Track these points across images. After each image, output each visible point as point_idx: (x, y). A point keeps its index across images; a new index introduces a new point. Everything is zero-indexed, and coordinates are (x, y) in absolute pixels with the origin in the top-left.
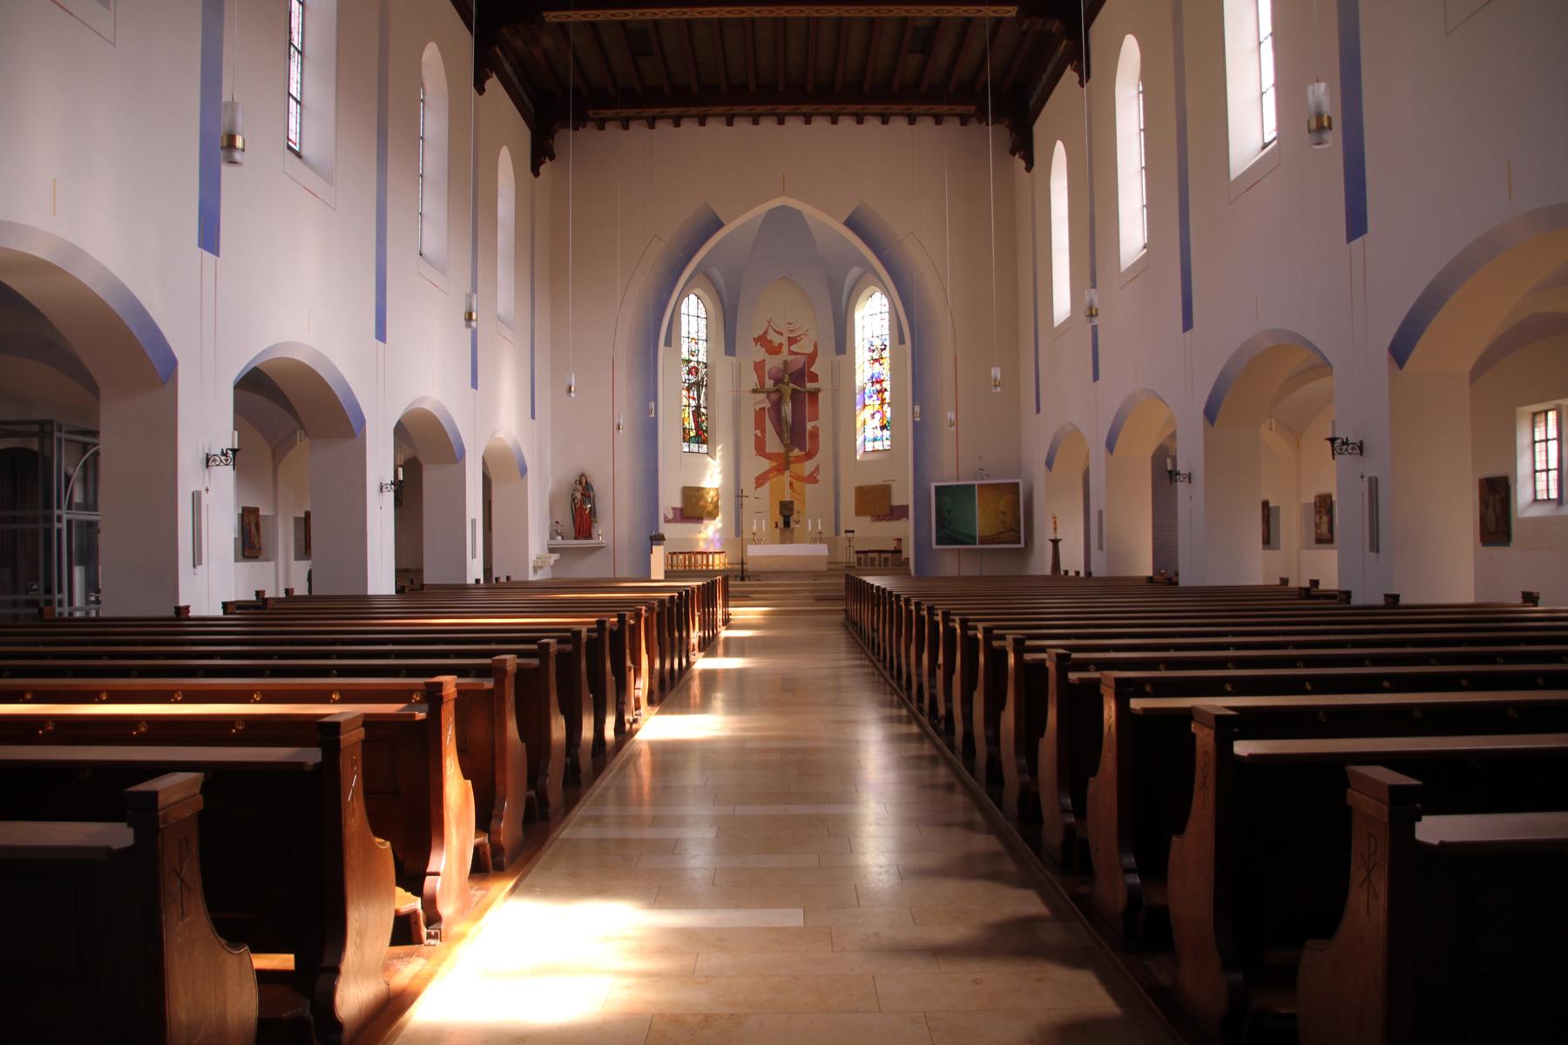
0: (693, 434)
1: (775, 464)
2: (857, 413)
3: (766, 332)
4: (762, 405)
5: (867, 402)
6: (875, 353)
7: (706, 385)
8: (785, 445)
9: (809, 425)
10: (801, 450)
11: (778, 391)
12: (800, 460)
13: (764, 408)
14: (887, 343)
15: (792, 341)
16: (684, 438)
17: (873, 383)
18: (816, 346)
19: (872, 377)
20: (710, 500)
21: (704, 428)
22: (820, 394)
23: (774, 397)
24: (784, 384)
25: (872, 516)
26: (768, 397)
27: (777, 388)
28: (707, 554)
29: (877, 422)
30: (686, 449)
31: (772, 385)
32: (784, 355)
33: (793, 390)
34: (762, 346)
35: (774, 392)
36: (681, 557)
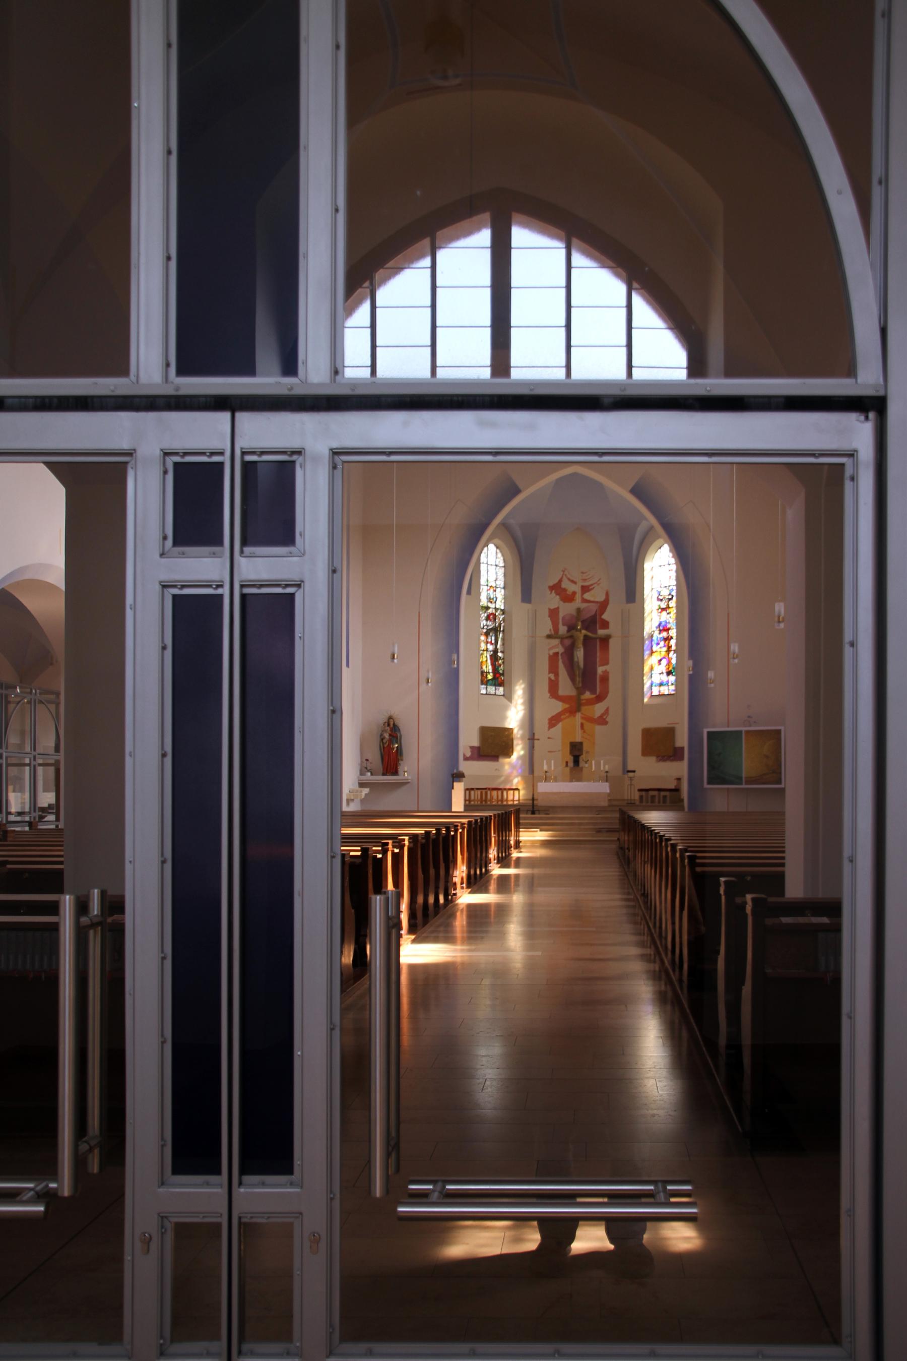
0: (490, 677)
1: (567, 706)
3: (560, 581)
5: (655, 648)
6: (664, 602)
7: (503, 631)
8: (577, 688)
9: (600, 670)
15: (585, 589)
18: (607, 594)
19: (660, 625)
21: (501, 672)
23: (568, 642)
26: (562, 643)
27: (569, 634)
28: (502, 790)
29: (663, 667)
30: (484, 692)
31: (565, 632)
32: (578, 603)
35: (567, 638)
36: (479, 792)
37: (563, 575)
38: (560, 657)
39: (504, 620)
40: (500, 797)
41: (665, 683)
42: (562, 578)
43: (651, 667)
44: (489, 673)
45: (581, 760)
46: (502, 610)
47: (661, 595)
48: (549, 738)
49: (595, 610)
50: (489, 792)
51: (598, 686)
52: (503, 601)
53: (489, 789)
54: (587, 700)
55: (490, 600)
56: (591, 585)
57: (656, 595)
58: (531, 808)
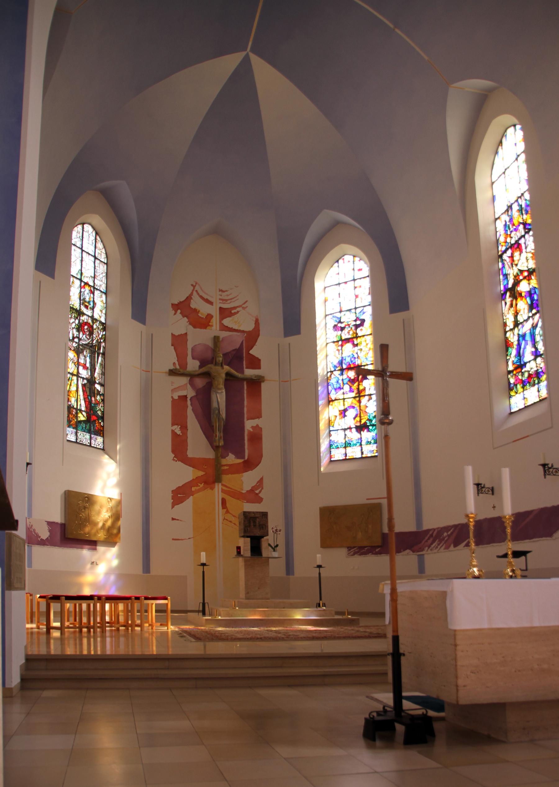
0: (82, 417)
1: (200, 473)
2: (320, 409)
3: (189, 298)
4: (183, 393)
5: (333, 396)
6: (346, 331)
7: (103, 354)
8: (216, 448)
9: (249, 425)
10: (238, 457)
11: (207, 374)
12: (235, 470)
13: (186, 397)
14: (368, 316)
15: (225, 313)
16: (69, 421)
17: (342, 370)
18: (257, 322)
19: (341, 363)
20: (100, 524)
21: (99, 413)
22: (263, 385)
23: (200, 383)
24: (216, 364)
25: (349, 548)
26: (191, 383)
27: (204, 369)
29: (350, 420)
30: (72, 438)
31: (197, 368)
32: (215, 330)
33: (228, 374)
34: (184, 316)
35: (199, 375)
37: (193, 290)
38: (189, 402)
39: (105, 338)
41: (355, 442)
42: (192, 294)
43: (327, 422)
44: (81, 411)
45: (264, 543)
46: (102, 324)
47: (343, 322)
48: (173, 519)
49: (240, 342)
51: (246, 447)
52: (104, 311)
53: (99, 598)
54: (230, 465)
55: (83, 301)
56: (235, 308)
57: (331, 322)
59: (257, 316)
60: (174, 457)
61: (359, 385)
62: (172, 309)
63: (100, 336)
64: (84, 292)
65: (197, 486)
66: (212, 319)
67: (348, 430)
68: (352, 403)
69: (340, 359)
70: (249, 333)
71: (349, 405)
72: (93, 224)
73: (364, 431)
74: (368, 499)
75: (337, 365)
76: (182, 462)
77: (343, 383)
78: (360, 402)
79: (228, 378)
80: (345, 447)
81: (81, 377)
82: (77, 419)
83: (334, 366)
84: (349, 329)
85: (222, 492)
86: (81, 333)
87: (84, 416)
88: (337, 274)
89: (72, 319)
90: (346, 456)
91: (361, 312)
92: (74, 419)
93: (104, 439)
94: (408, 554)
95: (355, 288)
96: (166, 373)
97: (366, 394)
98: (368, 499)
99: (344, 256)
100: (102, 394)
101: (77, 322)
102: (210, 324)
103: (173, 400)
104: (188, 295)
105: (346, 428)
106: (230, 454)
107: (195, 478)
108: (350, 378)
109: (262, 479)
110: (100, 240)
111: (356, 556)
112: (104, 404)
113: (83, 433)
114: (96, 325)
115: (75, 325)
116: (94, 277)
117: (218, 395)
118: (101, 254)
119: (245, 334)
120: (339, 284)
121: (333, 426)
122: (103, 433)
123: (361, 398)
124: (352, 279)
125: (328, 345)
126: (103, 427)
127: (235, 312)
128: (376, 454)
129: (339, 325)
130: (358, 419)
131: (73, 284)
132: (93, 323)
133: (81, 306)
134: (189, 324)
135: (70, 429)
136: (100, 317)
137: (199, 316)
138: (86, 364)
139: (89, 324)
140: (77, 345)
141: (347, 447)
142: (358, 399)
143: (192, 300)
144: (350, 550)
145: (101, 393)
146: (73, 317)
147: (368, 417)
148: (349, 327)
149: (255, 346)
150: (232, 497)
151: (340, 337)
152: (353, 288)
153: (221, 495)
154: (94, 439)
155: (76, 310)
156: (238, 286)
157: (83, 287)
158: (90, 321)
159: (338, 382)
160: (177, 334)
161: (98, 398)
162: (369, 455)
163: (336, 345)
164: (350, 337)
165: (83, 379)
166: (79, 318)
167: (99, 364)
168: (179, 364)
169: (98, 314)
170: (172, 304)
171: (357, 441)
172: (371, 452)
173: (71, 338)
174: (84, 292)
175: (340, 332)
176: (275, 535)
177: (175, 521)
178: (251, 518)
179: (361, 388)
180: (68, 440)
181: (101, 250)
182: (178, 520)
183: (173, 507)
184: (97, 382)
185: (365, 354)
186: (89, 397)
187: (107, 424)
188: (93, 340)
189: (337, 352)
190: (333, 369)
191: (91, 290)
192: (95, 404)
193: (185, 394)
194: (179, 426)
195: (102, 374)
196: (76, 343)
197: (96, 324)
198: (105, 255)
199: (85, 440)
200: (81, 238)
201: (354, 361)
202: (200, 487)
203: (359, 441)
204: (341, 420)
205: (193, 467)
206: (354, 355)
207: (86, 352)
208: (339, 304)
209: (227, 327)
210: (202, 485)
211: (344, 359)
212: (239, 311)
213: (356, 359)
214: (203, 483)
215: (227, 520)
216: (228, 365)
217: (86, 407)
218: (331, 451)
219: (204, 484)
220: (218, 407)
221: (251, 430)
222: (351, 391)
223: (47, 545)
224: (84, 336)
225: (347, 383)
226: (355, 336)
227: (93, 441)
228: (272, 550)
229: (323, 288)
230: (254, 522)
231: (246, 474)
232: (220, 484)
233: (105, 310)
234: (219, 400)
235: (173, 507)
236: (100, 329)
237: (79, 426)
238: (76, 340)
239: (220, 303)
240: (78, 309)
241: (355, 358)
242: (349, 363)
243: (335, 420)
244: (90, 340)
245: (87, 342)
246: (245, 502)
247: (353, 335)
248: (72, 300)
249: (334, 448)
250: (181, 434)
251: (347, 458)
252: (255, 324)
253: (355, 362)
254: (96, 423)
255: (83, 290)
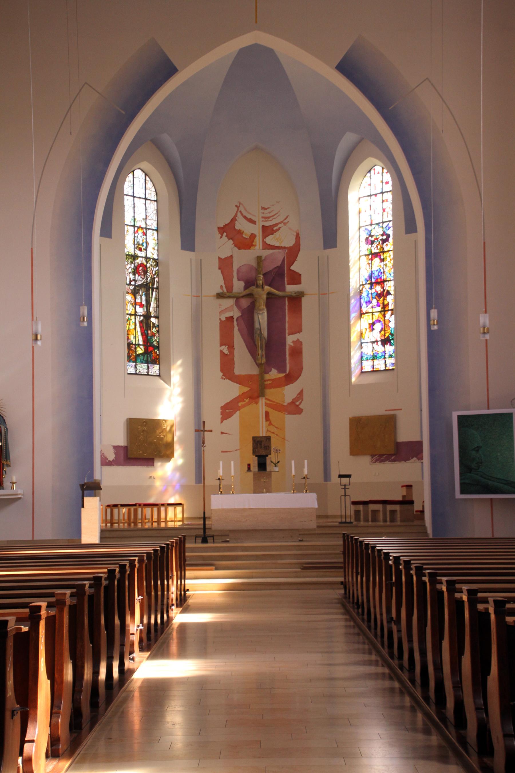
0: (140, 351)
1: (246, 389)
3: (234, 220)
5: (364, 309)
6: (375, 245)
7: (157, 288)
8: (259, 365)
9: (290, 340)
11: (250, 295)
12: (278, 384)
13: (232, 317)
15: (267, 231)
16: (129, 356)
17: (371, 284)
18: (298, 237)
19: (370, 277)
21: (155, 344)
22: (304, 300)
23: (245, 303)
24: (257, 286)
25: (372, 456)
26: (237, 304)
27: (248, 291)
29: (376, 335)
30: (133, 371)
32: (258, 250)
33: (269, 294)
36: (124, 510)
37: (238, 211)
38: (235, 323)
40: (109, 518)
41: (380, 355)
42: (236, 215)
43: (359, 334)
44: (139, 345)
47: (373, 236)
48: (222, 433)
50: (140, 510)
51: (288, 361)
52: (156, 248)
56: (276, 225)
57: (364, 235)
58: (201, 532)
59: (298, 230)
60: (223, 375)
61: (384, 300)
62: (218, 233)
63: (154, 273)
64: (137, 236)
65: (244, 401)
66: (255, 239)
67: (376, 343)
68: (379, 317)
69: (370, 272)
70: (290, 249)
71: (376, 319)
72: (142, 168)
73: (387, 345)
74: (386, 410)
75: (368, 279)
76: (230, 379)
77: (372, 297)
78: (384, 316)
79: (270, 296)
80: (373, 360)
81: (138, 315)
82: (136, 353)
83: (365, 279)
84: (378, 243)
85: (265, 405)
86: (137, 275)
87: (142, 350)
88: (369, 185)
89: (128, 265)
90: (373, 368)
91: (387, 227)
92: (133, 354)
93: (159, 366)
94: (414, 462)
95: (383, 201)
96: (214, 296)
97: (390, 308)
98: (386, 410)
99: (375, 166)
100: (157, 325)
101: (133, 266)
102: (254, 244)
103: (221, 322)
104: (232, 217)
105: (374, 341)
106: (273, 369)
107: (241, 394)
108: (377, 292)
109: (302, 391)
110: (149, 180)
111: (377, 463)
112: (159, 334)
113: (141, 364)
114: (150, 263)
115: (131, 270)
116: (146, 219)
117: (259, 316)
118: (151, 193)
119: (286, 251)
120: (371, 196)
121: (364, 339)
122: (159, 361)
123: (386, 312)
124: (381, 191)
125: (361, 258)
126: (159, 355)
127: (276, 229)
128: (394, 368)
129: (370, 238)
130: (383, 332)
131: (128, 232)
132: (147, 262)
133: (136, 250)
134: (234, 246)
135: (130, 363)
136: (153, 254)
137: (243, 237)
138: (142, 303)
139: (143, 264)
140: (133, 287)
141: (375, 359)
142: (383, 313)
143: (236, 222)
144: (372, 458)
145: (156, 325)
146: (129, 263)
147: (391, 332)
148: (378, 241)
149: (296, 262)
150: (275, 410)
151: (370, 251)
152: (381, 201)
153: (265, 408)
154: (151, 368)
155: (132, 256)
156: (279, 202)
157: (136, 232)
158: (144, 262)
159: (368, 295)
160: (223, 257)
161: (154, 330)
162: (391, 368)
163: (367, 259)
164: (378, 251)
165: (140, 316)
166: (134, 262)
167: (153, 299)
168: (226, 287)
169: (151, 252)
170: (219, 228)
171: (382, 354)
172: (392, 365)
173: (128, 283)
174: (137, 236)
175: (370, 246)
176: (276, 454)
177: (224, 435)
178: (258, 441)
179: (386, 303)
180: (129, 374)
181: (151, 190)
182: (226, 434)
183: (222, 422)
184: (152, 316)
185: (389, 269)
186: (146, 331)
187: (162, 353)
188: (147, 279)
189: (368, 265)
190: (364, 283)
191: (143, 232)
192: (151, 336)
193: (232, 315)
194: (227, 346)
195: (156, 307)
196: (133, 285)
197: (149, 262)
198: (155, 192)
199: (143, 370)
200: (132, 186)
201: (380, 276)
202: (246, 402)
203: (384, 354)
204: (370, 333)
205: (240, 384)
206: (381, 270)
207: (142, 291)
208: (370, 216)
209: (269, 244)
210: (247, 401)
211: (373, 272)
212: (281, 228)
213: (383, 274)
214: (248, 399)
215: (270, 431)
216: (270, 285)
217: (144, 341)
218: (362, 363)
219: (249, 400)
220: (259, 328)
221: (292, 344)
222: (378, 305)
223: (113, 465)
224: (139, 277)
225: (375, 298)
226: (382, 251)
227: (150, 370)
228: (274, 465)
229: (358, 198)
230: (261, 444)
231: (287, 387)
232: (264, 399)
233: (157, 246)
234: (260, 320)
235: (222, 422)
236: (153, 266)
237: (138, 359)
238: (133, 283)
239: (263, 221)
240: (133, 254)
241: (381, 273)
242: (376, 277)
243: (366, 333)
244: (145, 279)
245: (142, 282)
246: (286, 414)
247: (380, 250)
248: (127, 248)
249: (365, 359)
250: (228, 354)
251: (374, 369)
252: (296, 238)
253: (382, 277)
254: (152, 353)
255: (136, 235)
